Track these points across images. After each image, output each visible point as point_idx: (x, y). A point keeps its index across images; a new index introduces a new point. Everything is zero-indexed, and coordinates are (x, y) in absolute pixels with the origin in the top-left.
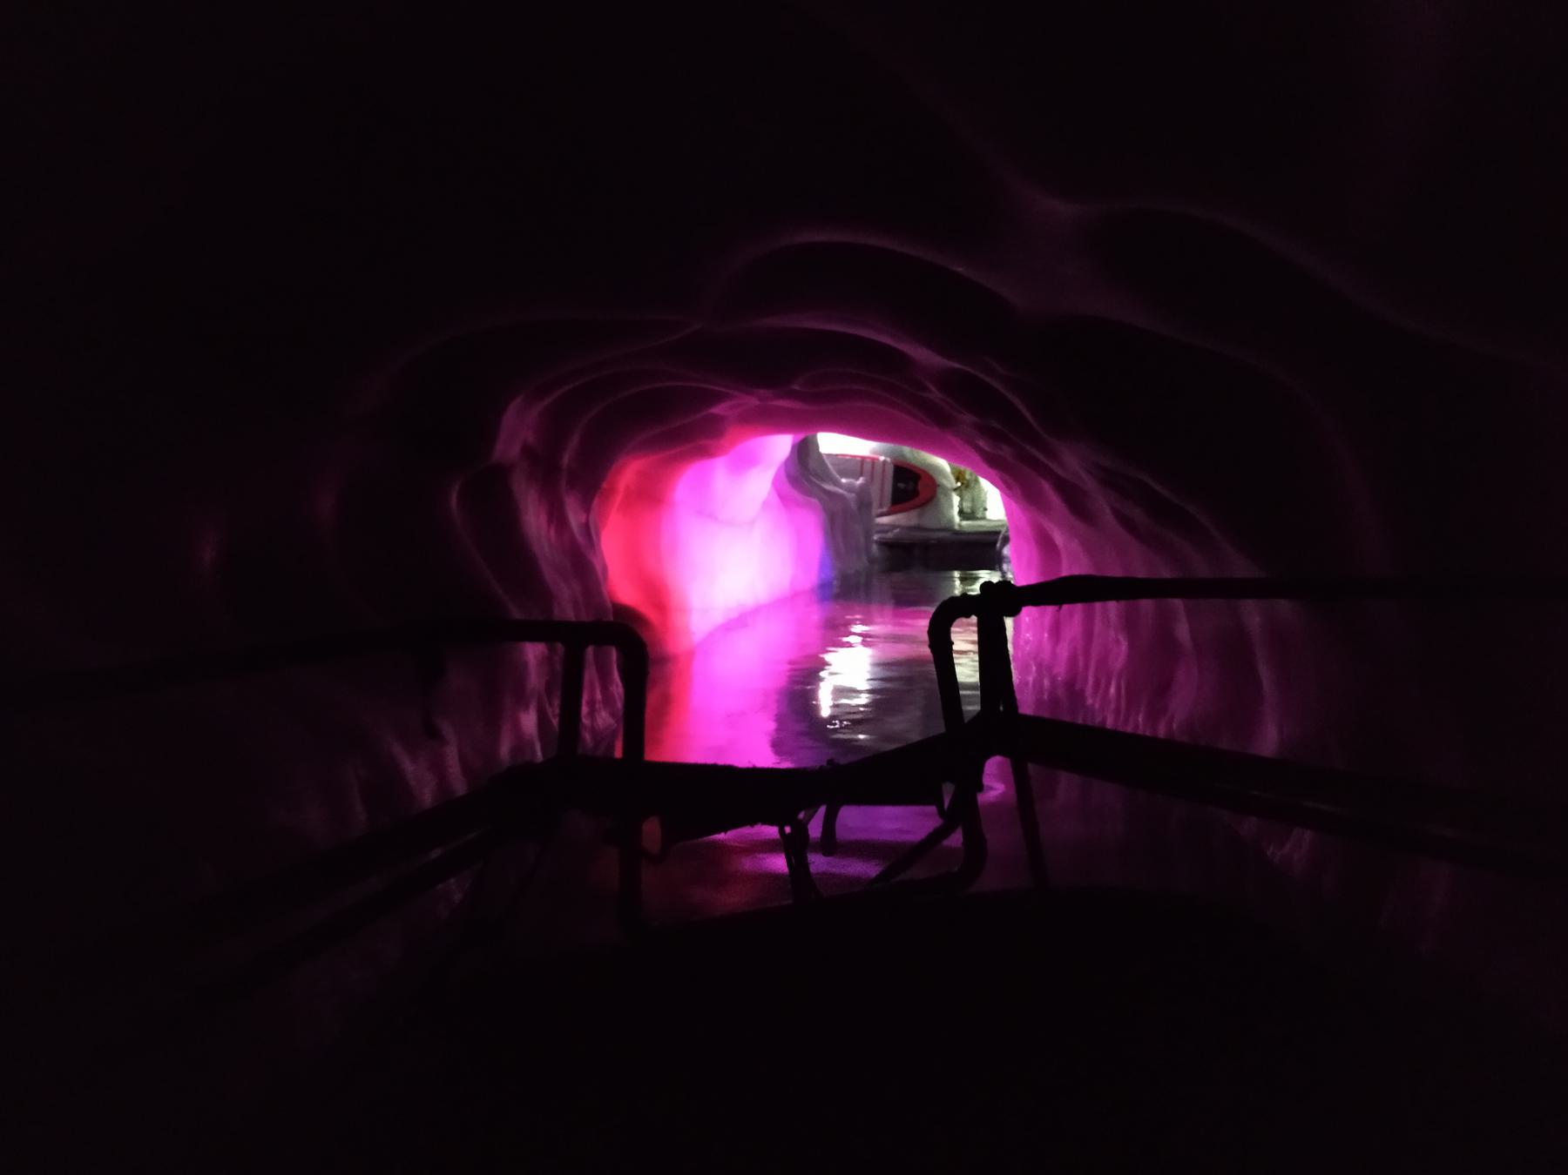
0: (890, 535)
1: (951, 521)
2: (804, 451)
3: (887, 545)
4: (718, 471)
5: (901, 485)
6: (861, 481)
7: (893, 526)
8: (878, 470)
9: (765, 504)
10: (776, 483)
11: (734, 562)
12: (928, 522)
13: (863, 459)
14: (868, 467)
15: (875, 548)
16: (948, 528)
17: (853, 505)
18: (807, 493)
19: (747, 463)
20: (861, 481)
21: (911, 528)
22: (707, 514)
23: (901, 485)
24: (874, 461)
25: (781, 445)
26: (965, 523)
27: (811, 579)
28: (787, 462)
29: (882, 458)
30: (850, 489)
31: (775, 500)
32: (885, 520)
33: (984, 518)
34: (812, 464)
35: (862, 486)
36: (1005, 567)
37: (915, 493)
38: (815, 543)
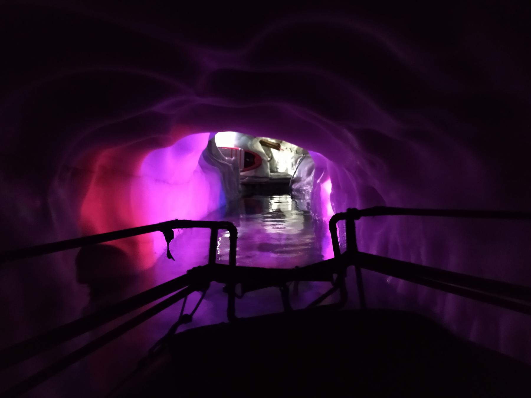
0: (244, 180)
1: (267, 174)
2: (211, 143)
3: (243, 184)
4: (168, 154)
5: (248, 160)
6: (233, 158)
7: (245, 177)
8: (238, 153)
9: (195, 172)
10: (200, 163)
11: (175, 187)
12: (259, 174)
13: (232, 149)
14: (234, 152)
15: (240, 186)
16: (267, 177)
17: (232, 169)
18: (213, 164)
19: (184, 150)
20: (233, 158)
21: (252, 177)
22: (160, 180)
23: (248, 160)
24: (236, 150)
25: (203, 138)
26: (272, 174)
27: (222, 208)
28: (206, 149)
29: (240, 149)
30: (229, 162)
31: (199, 169)
32: (242, 174)
33: (277, 172)
34: (214, 152)
35: (234, 160)
36: (293, 193)
37: (254, 163)
38: (218, 188)
